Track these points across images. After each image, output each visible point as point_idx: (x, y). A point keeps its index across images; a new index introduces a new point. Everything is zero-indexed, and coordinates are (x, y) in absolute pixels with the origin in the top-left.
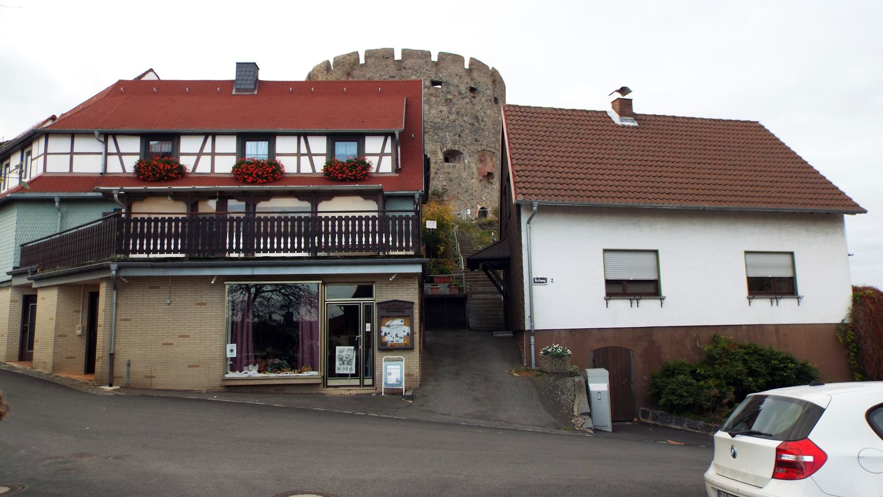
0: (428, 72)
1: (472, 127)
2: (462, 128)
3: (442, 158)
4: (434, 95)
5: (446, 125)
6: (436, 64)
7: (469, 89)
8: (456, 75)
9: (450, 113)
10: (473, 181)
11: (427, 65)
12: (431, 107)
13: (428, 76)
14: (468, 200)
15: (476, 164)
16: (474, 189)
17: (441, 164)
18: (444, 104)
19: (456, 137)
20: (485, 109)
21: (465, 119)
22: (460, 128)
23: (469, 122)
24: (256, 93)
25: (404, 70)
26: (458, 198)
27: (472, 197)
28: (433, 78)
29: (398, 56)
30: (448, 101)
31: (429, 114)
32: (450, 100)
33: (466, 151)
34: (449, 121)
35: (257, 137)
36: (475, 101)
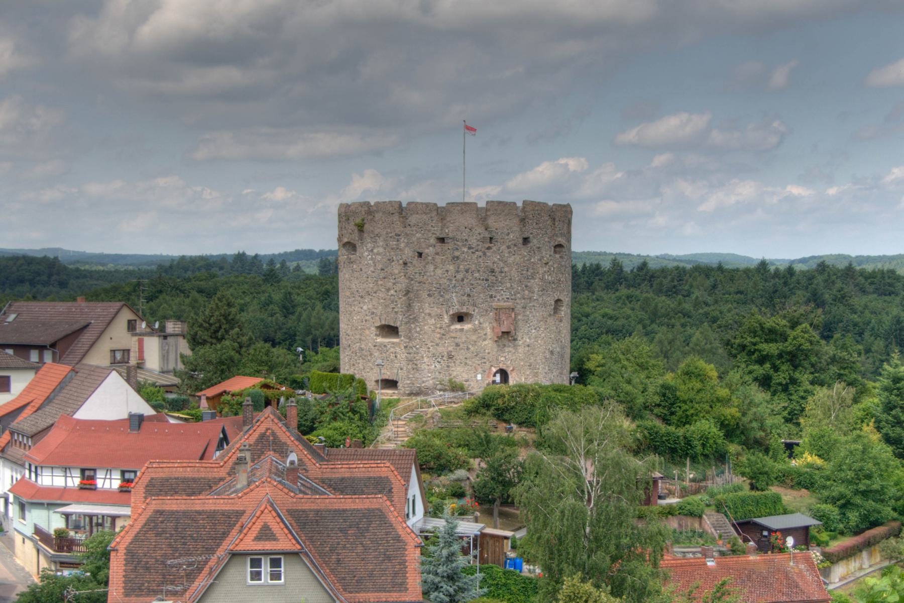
9: (458, 272)
19: (465, 298)
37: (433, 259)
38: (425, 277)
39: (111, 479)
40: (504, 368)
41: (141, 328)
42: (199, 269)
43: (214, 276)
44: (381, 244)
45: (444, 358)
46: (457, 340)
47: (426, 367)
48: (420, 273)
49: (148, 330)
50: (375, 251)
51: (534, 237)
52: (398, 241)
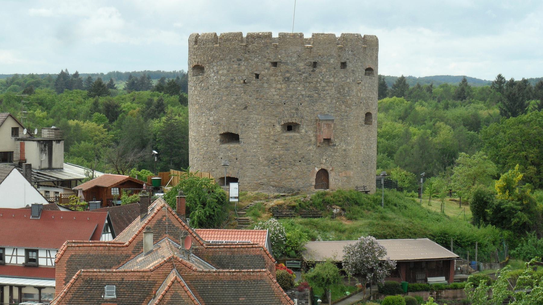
24: (39, 218)
35: (33, 251)
37: (268, 79)
39: (17, 256)
40: (325, 168)
41: (23, 134)
42: (530, 134)
49: (28, 136)
50: (220, 72)
51: (350, 62)
52: (239, 65)
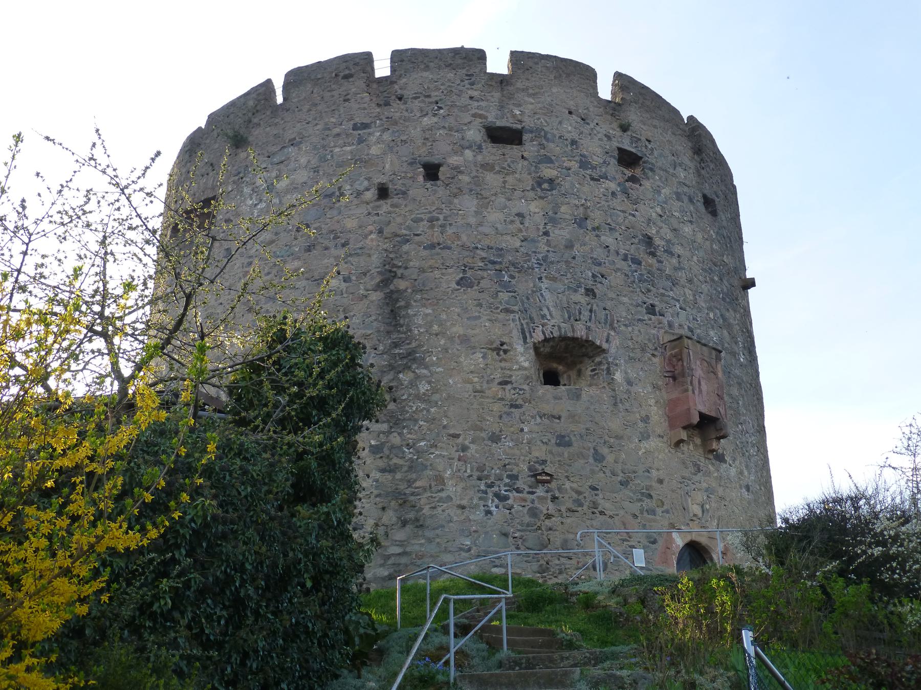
0: (476, 104)
1: (634, 267)
2: (597, 268)
3: (526, 364)
4: (497, 168)
5: (540, 256)
6: (501, 82)
7: (616, 154)
8: (570, 113)
9: (552, 220)
10: (653, 443)
11: (472, 84)
12: (484, 202)
13: (474, 116)
14: (635, 516)
15: (655, 387)
16: (654, 473)
17: (525, 387)
18: (531, 194)
19: (580, 297)
20: (672, 220)
21: (608, 239)
22: (590, 269)
23: (622, 251)
25: (396, 104)
26: (595, 505)
27: (651, 504)
28: (490, 119)
29: (382, 69)
30: (545, 186)
31: (480, 224)
32: (551, 181)
33: (616, 342)
34: (548, 243)
36: (635, 190)
37: (477, 181)
38: (450, 231)
40: (703, 540)
43: (60, 513)
44: (303, 161)
45: (520, 484)
46: (562, 427)
47: (454, 513)
48: (431, 220)
